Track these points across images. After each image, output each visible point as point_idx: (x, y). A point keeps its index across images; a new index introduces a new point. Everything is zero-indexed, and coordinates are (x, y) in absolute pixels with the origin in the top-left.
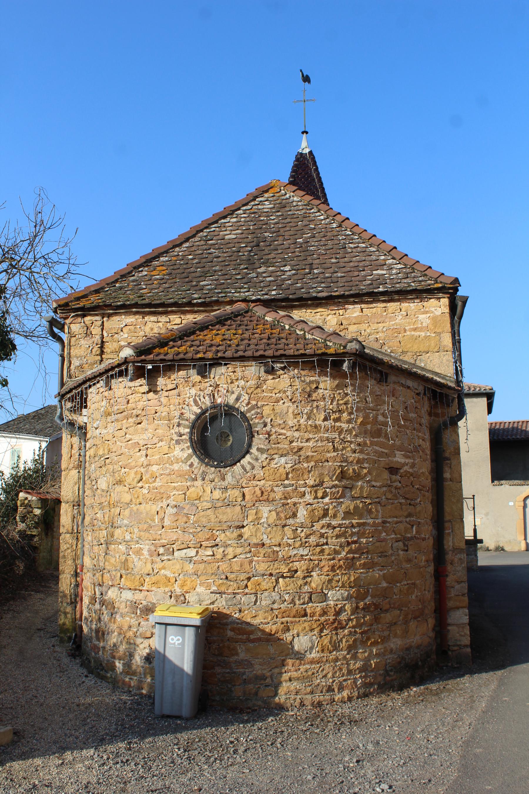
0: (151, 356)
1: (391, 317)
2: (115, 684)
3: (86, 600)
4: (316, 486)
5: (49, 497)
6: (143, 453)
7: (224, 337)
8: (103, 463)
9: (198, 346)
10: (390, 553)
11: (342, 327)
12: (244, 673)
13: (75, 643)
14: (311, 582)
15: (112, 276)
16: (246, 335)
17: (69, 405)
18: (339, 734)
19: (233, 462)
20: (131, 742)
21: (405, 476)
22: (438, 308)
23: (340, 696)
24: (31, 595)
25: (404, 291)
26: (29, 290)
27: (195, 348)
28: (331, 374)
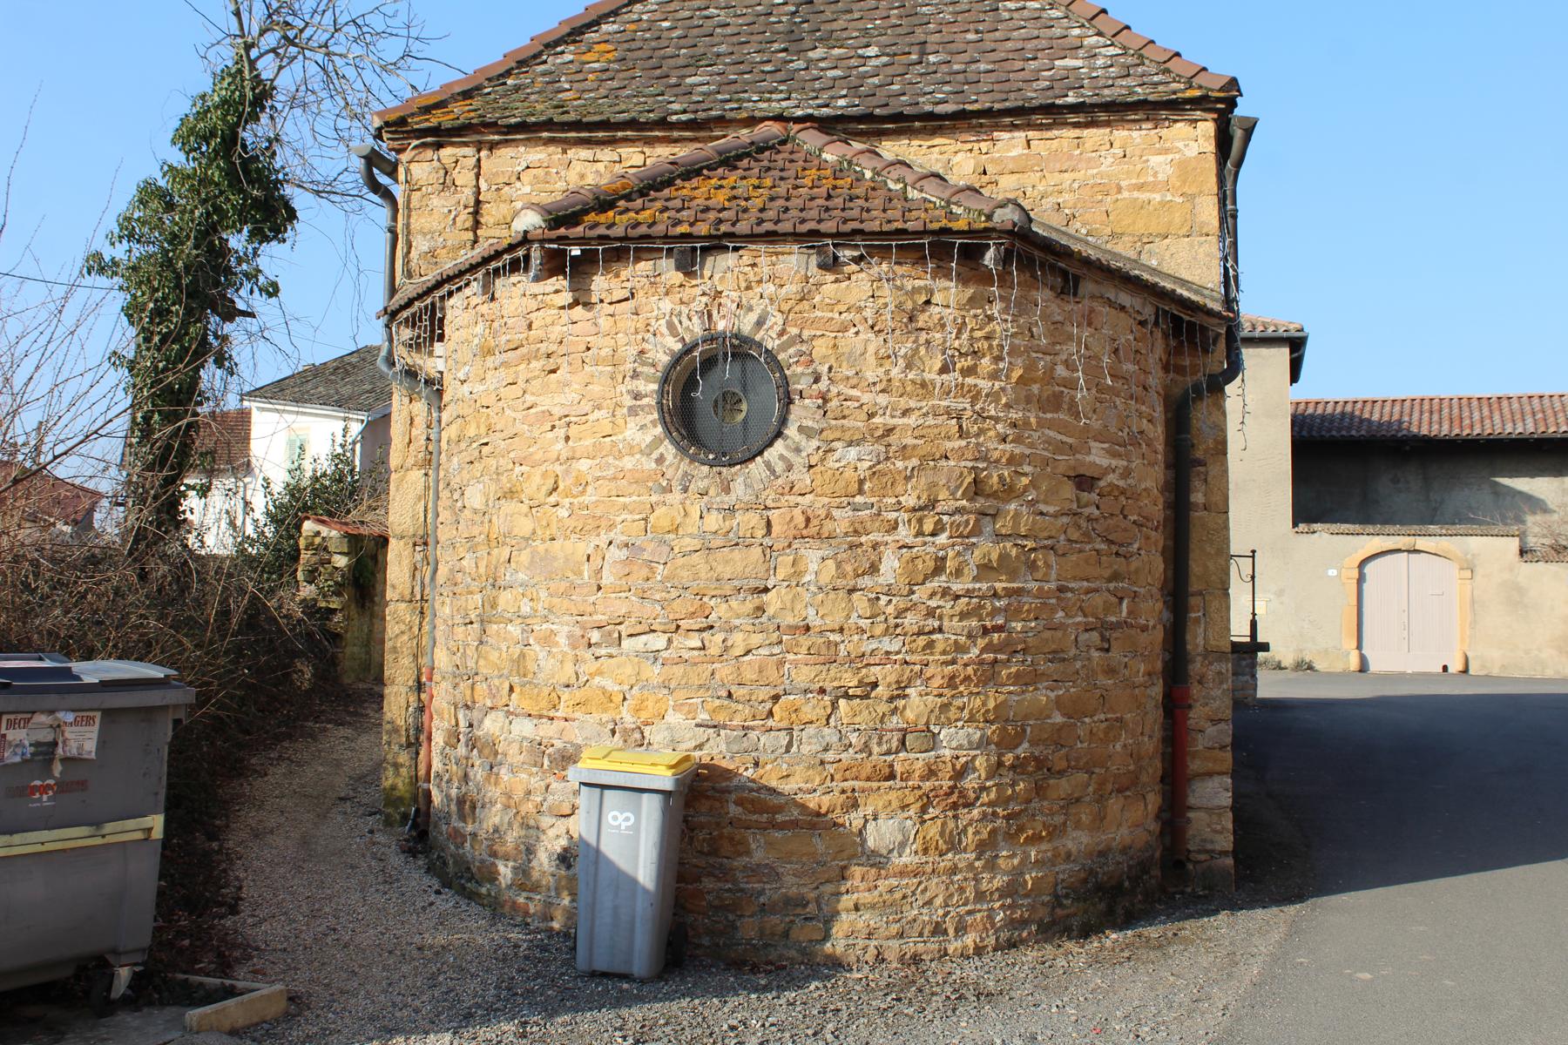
0: (579, 230)
1: (1090, 159)
2: (496, 908)
3: (438, 739)
4: (921, 509)
5: (364, 531)
6: (561, 432)
7: (735, 192)
8: (476, 453)
9: (678, 211)
10: (1071, 654)
11: (985, 179)
12: (762, 892)
13: (415, 826)
14: (905, 707)
15: (499, 63)
16: (781, 190)
17: (407, 333)
18: (955, 1019)
19: (747, 455)
20: (526, 1022)
21: (1109, 494)
22: (1192, 143)
23: (958, 944)
24: (325, 730)
25: (1121, 104)
26: (324, 94)
27: (672, 213)
28: (958, 275)
